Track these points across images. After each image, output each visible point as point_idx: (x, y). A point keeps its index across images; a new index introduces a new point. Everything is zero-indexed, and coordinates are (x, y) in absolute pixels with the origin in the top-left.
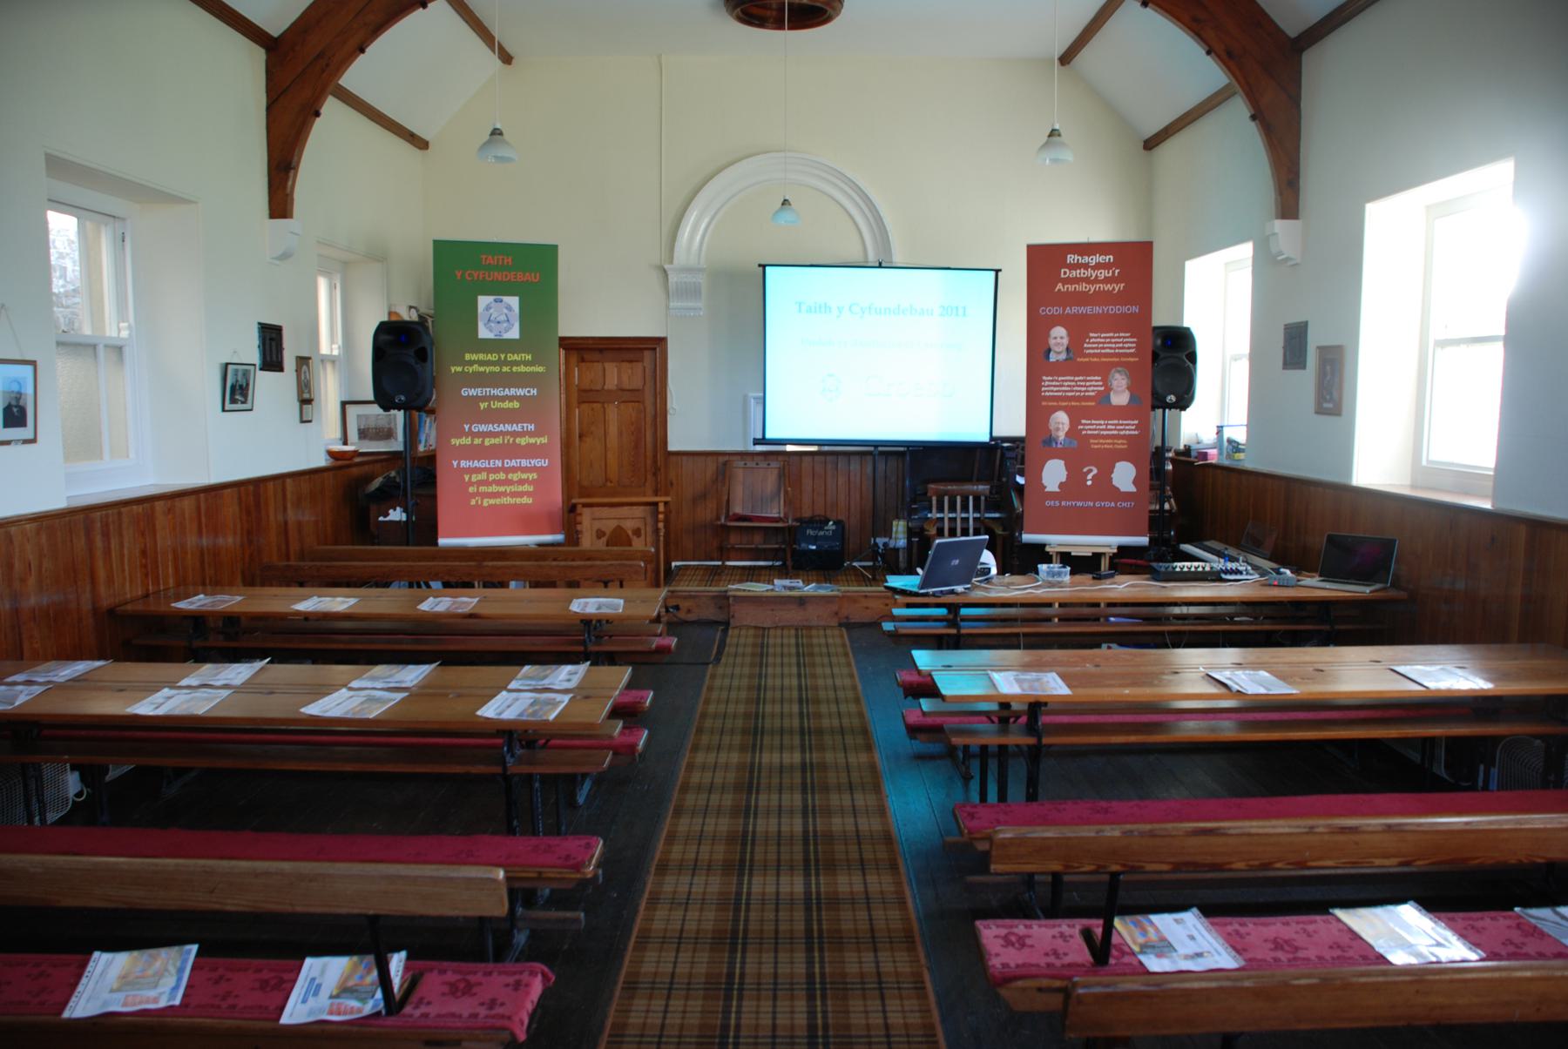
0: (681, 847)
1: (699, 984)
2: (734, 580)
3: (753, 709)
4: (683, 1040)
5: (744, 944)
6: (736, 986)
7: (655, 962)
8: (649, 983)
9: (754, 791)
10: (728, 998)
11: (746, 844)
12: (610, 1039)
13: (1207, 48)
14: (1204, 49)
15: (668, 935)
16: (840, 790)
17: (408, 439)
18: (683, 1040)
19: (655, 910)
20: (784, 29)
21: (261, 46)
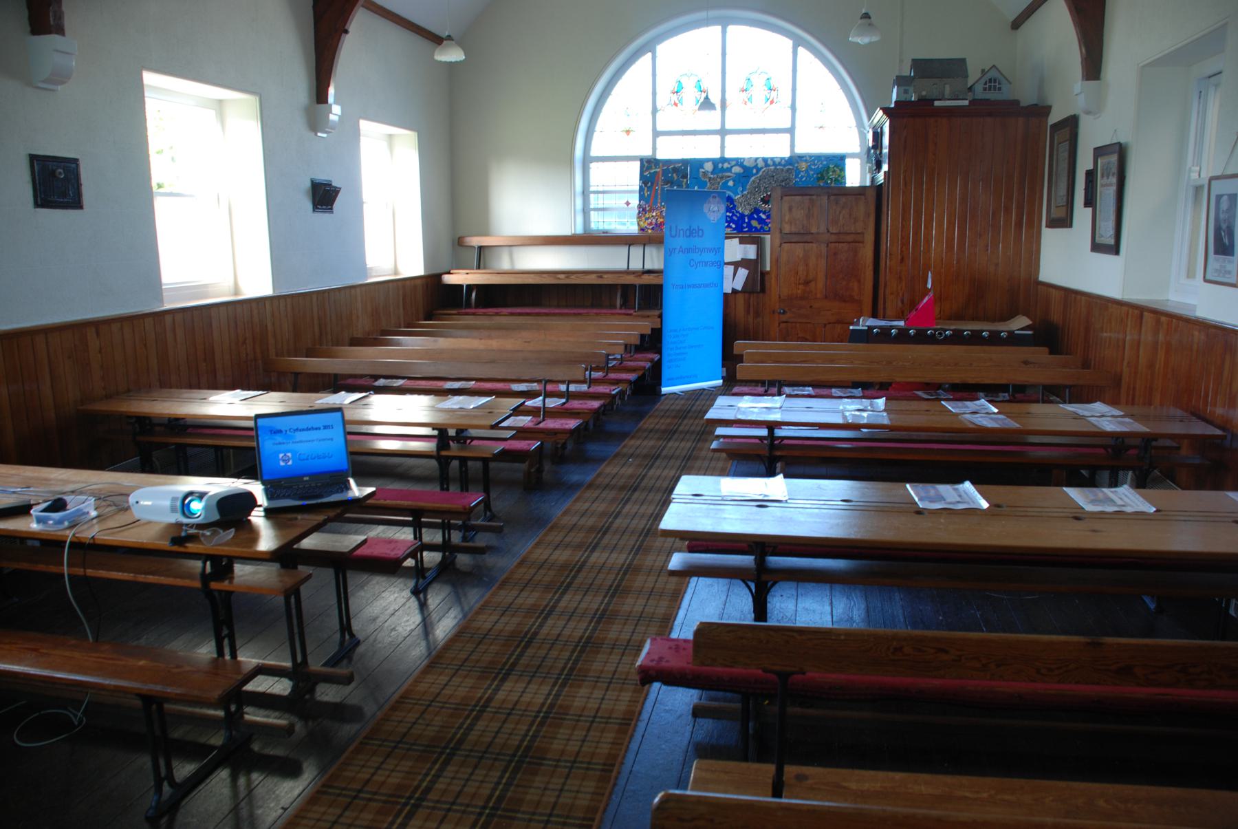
0: (668, 587)
1: (589, 681)
2: (714, 469)
3: (700, 445)
4: (554, 763)
5: (595, 614)
6: (563, 677)
7: (620, 700)
8: (611, 723)
9: (646, 530)
10: (618, 586)
11: (570, 668)
12: (630, 722)
13: (343, 35)
14: (345, 37)
15: (634, 651)
16: (750, 293)
17: (880, 138)
18: (554, 763)
19: (675, 590)
20: (614, 307)
21: (717, 134)
